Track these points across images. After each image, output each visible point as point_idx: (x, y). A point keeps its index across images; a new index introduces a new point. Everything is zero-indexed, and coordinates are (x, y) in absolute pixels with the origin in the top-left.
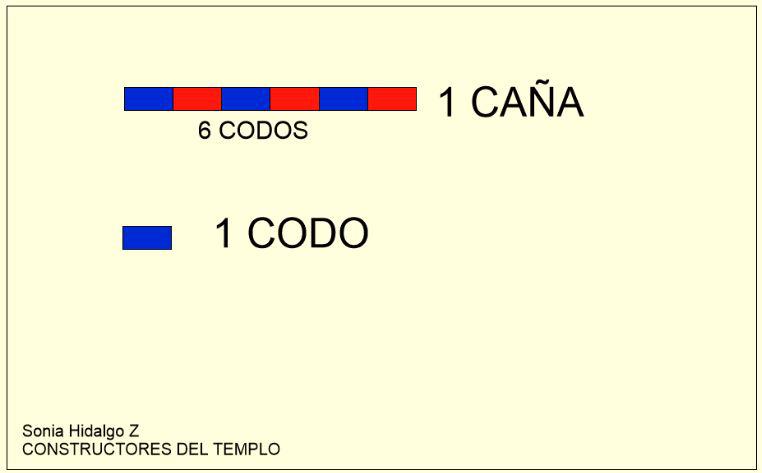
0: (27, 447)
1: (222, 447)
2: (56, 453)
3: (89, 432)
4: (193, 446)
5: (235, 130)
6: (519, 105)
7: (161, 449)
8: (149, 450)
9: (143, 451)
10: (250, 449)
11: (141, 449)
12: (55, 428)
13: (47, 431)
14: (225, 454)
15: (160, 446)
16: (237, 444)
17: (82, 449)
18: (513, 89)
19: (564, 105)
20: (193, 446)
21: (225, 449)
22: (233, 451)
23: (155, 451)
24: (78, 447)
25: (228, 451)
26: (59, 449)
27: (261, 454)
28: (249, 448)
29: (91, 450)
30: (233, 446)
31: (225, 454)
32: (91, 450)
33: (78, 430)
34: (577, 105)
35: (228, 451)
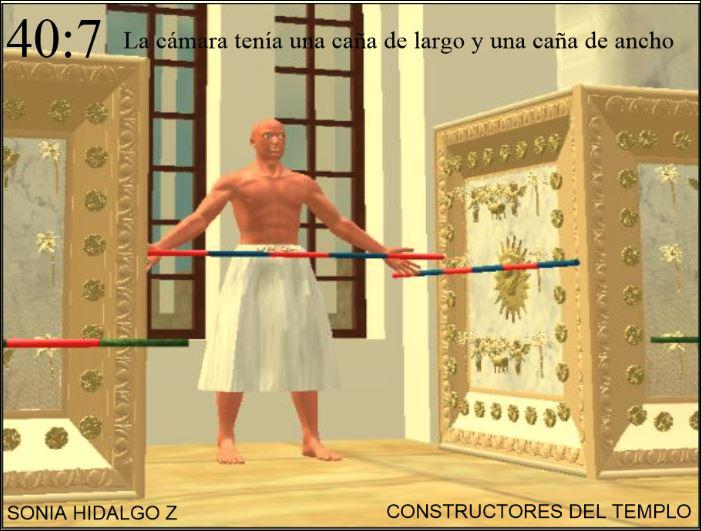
0: (138, 510)
1: (622, 510)
2: (426, 516)
3: (659, 509)
4: (543, 508)
5: (399, 511)
6: (115, 514)
7: (551, 511)
8: (536, 513)
9: (529, 514)
10: (655, 512)
11: (526, 511)
12: (272, 37)
13: (475, 514)
14: (626, 517)
15: (549, 508)
16: (639, 506)
17: (457, 511)
18: (112, 507)
19: (58, 514)
20: (588, 508)
21: (627, 511)
22: (636, 514)
23: (543, 514)
24: (453, 509)
25: (629, 514)
26: (430, 511)
27: (668, 517)
28: (499, 43)
29: (467, 513)
30: (636, 508)
31: (626, 517)
32: (467, 513)
33: (84, 513)
34: (63, 514)
35: (629, 514)
